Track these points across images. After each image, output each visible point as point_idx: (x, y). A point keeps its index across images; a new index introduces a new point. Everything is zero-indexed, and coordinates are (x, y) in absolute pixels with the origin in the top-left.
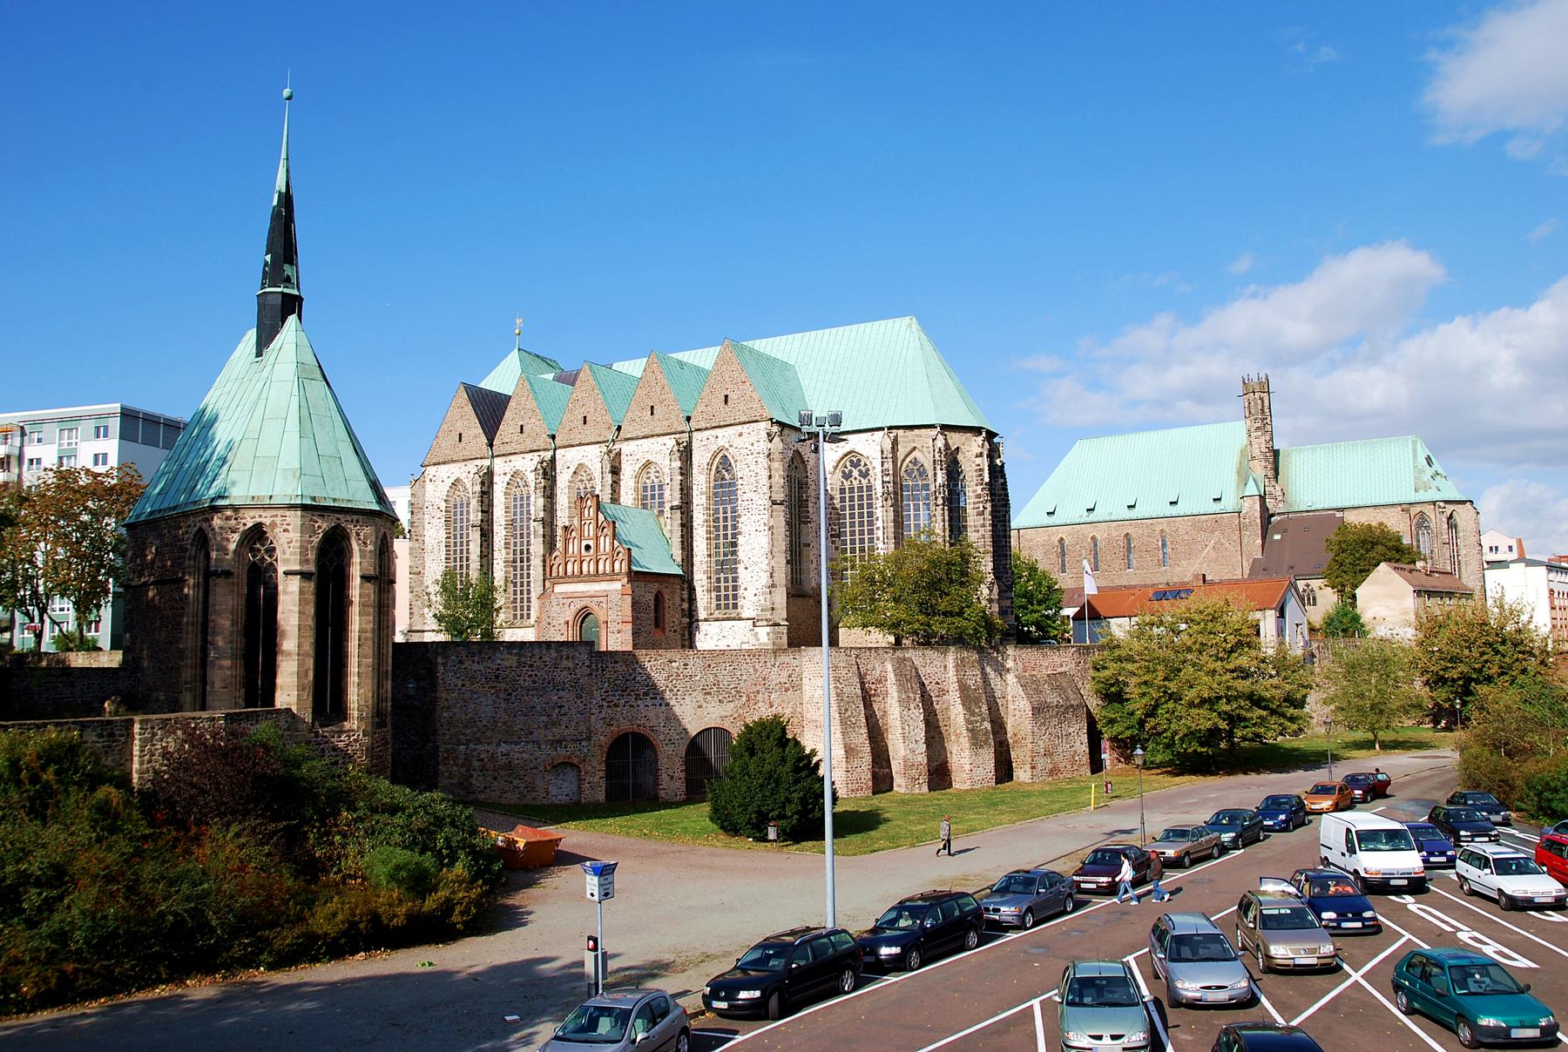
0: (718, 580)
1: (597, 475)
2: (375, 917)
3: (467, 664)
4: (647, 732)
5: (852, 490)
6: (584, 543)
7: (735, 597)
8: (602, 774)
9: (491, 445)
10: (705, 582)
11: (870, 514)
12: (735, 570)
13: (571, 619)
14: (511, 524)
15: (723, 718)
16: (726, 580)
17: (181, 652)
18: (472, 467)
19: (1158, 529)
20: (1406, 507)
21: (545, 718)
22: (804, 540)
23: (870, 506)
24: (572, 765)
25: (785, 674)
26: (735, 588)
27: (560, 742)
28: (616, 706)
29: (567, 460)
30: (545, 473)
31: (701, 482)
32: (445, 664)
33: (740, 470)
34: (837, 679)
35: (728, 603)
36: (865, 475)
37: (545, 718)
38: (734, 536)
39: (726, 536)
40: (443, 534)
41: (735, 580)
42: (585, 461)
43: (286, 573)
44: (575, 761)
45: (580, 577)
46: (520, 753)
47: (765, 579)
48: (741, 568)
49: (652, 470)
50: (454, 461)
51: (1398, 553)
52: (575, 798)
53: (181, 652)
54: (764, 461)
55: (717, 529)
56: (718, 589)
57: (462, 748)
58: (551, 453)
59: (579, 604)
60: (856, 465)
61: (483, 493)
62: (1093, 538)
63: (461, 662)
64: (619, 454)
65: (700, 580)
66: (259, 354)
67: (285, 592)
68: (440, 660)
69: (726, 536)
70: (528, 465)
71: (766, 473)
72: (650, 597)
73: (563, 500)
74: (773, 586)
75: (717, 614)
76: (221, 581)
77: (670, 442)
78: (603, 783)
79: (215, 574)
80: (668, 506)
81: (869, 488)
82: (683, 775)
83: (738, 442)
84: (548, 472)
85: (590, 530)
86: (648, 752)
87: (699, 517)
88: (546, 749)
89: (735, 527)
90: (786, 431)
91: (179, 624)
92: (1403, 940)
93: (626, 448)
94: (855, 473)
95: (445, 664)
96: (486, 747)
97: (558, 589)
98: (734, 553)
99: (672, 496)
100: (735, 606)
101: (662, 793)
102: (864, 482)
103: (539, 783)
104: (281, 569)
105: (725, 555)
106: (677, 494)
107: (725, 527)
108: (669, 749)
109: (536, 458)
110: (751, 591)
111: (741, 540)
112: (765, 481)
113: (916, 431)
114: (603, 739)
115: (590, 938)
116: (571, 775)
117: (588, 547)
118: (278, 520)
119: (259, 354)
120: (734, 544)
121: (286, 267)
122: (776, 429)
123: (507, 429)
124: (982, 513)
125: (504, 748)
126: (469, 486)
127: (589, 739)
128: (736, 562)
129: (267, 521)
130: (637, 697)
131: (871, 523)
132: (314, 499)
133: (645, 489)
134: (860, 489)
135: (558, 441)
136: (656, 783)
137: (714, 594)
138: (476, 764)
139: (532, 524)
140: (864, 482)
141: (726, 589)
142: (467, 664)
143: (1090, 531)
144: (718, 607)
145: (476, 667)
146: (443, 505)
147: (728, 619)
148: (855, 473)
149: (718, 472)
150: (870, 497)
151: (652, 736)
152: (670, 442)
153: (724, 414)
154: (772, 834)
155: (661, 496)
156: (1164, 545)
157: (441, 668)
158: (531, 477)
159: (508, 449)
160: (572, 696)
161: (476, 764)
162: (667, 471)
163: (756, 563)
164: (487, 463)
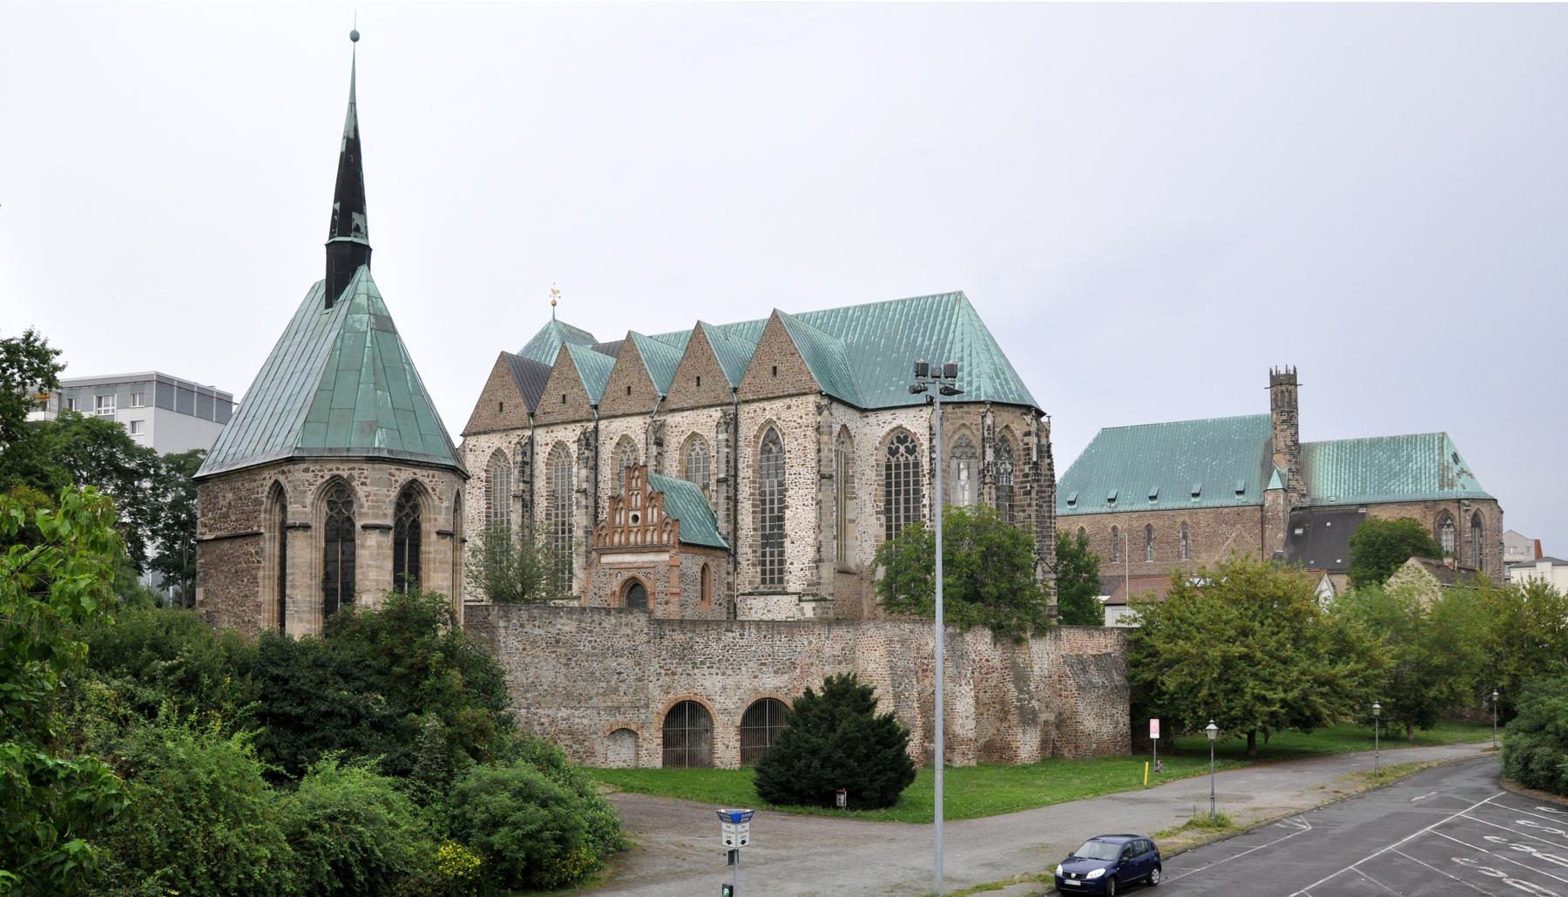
0: (764, 554)
1: (641, 446)
5: (898, 466)
7: (781, 571)
8: (660, 741)
10: (750, 556)
11: (917, 491)
12: (781, 545)
14: (552, 496)
15: (778, 689)
16: (772, 555)
17: (258, 606)
18: (514, 437)
19: (1179, 520)
20: (1429, 504)
22: (849, 516)
23: (916, 483)
24: (630, 732)
25: (838, 647)
26: (782, 562)
27: (618, 708)
28: (674, 674)
29: (611, 430)
30: (588, 444)
31: (748, 455)
33: (789, 443)
34: (891, 653)
35: (773, 578)
36: (911, 451)
38: (781, 510)
39: (772, 510)
40: (483, 504)
41: (781, 554)
43: (365, 527)
44: (633, 727)
46: (582, 719)
47: (811, 553)
48: (787, 543)
49: (697, 443)
50: (493, 431)
51: (1428, 551)
52: (632, 765)
53: (258, 606)
54: (811, 433)
55: (763, 502)
56: (763, 563)
57: (523, 711)
58: (592, 425)
59: (626, 575)
60: (902, 441)
61: (524, 463)
62: (1114, 528)
63: (522, 626)
64: (663, 425)
65: (746, 552)
66: (329, 305)
67: (363, 546)
68: (502, 624)
69: (772, 510)
70: (569, 435)
71: (812, 448)
72: (697, 569)
73: (606, 472)
74: (820, 560)
75: (762, 588)
76: (300, 533)
77: (716, 414)
78: (660, 750)
79: (294, 527)
80: (713, 481)
81: (916, 465)
82: (738, 744)
83: (785, 414)
84: (590, 442)
85: (637, 501)
86: (703, 720)
87: (745, 491)
88: (604, 715)
89: (781, 501)
90: (835, 405)
91: (255, 577)
93: (672, 419)
94: (902, 449)
95: (506, 628)
97: (605, 559)
98: (781, 527)
99: (718, 469)
100: (781, 581)
101: (717, 762)
102: (911, 459)
103: (599, 748)
104: (358, 525)
105: (772, 528)
106: (723, 467)
107: (772, 502)
111: (788, 514)
112: (812, 454)
113: (966, 409)
114: (661, 706)
115: (724, 886)
116: (628, 742)
117: (636, 518)
118: (356, 473)
119: (329, 305)
120: (781, 519)
121: (355, 215)
122: (825, 402)
123: (550, 400)
124: (1029, 493)
125: (564, 713)
126: (510, 456)
127: (647, 706)
128: (783, 536)
129: (345, 474)
130: (694, 666)
131: (917, 500)
132: (390, 452)
133: (689, 461)
134: (907, 466)
135: (602, 409)
136: (712, 752)
137: (759, 569)
138: (537, 728)
139: (575, 495)
140: (911, 459)
141: (772, 563)
142: (528, 628)
143: (1111, 522)
144: (763, 581)
145: (537, 631)
147: (774, 594)
148: (902, 449)
149: (764, 445)
150: (916, 474)
151: (708, 705)
152: (716, 414)
153: (771, 385)
154: (842, 799)
155: (706, 468)
156: (1185, 537)
157: (502, 631)
158: (573, 448)
159: (551, 419)
160: (630, 663)
161: (537, 728)
162: (712, 443)
163: (803, 538)
164: (529, 433)
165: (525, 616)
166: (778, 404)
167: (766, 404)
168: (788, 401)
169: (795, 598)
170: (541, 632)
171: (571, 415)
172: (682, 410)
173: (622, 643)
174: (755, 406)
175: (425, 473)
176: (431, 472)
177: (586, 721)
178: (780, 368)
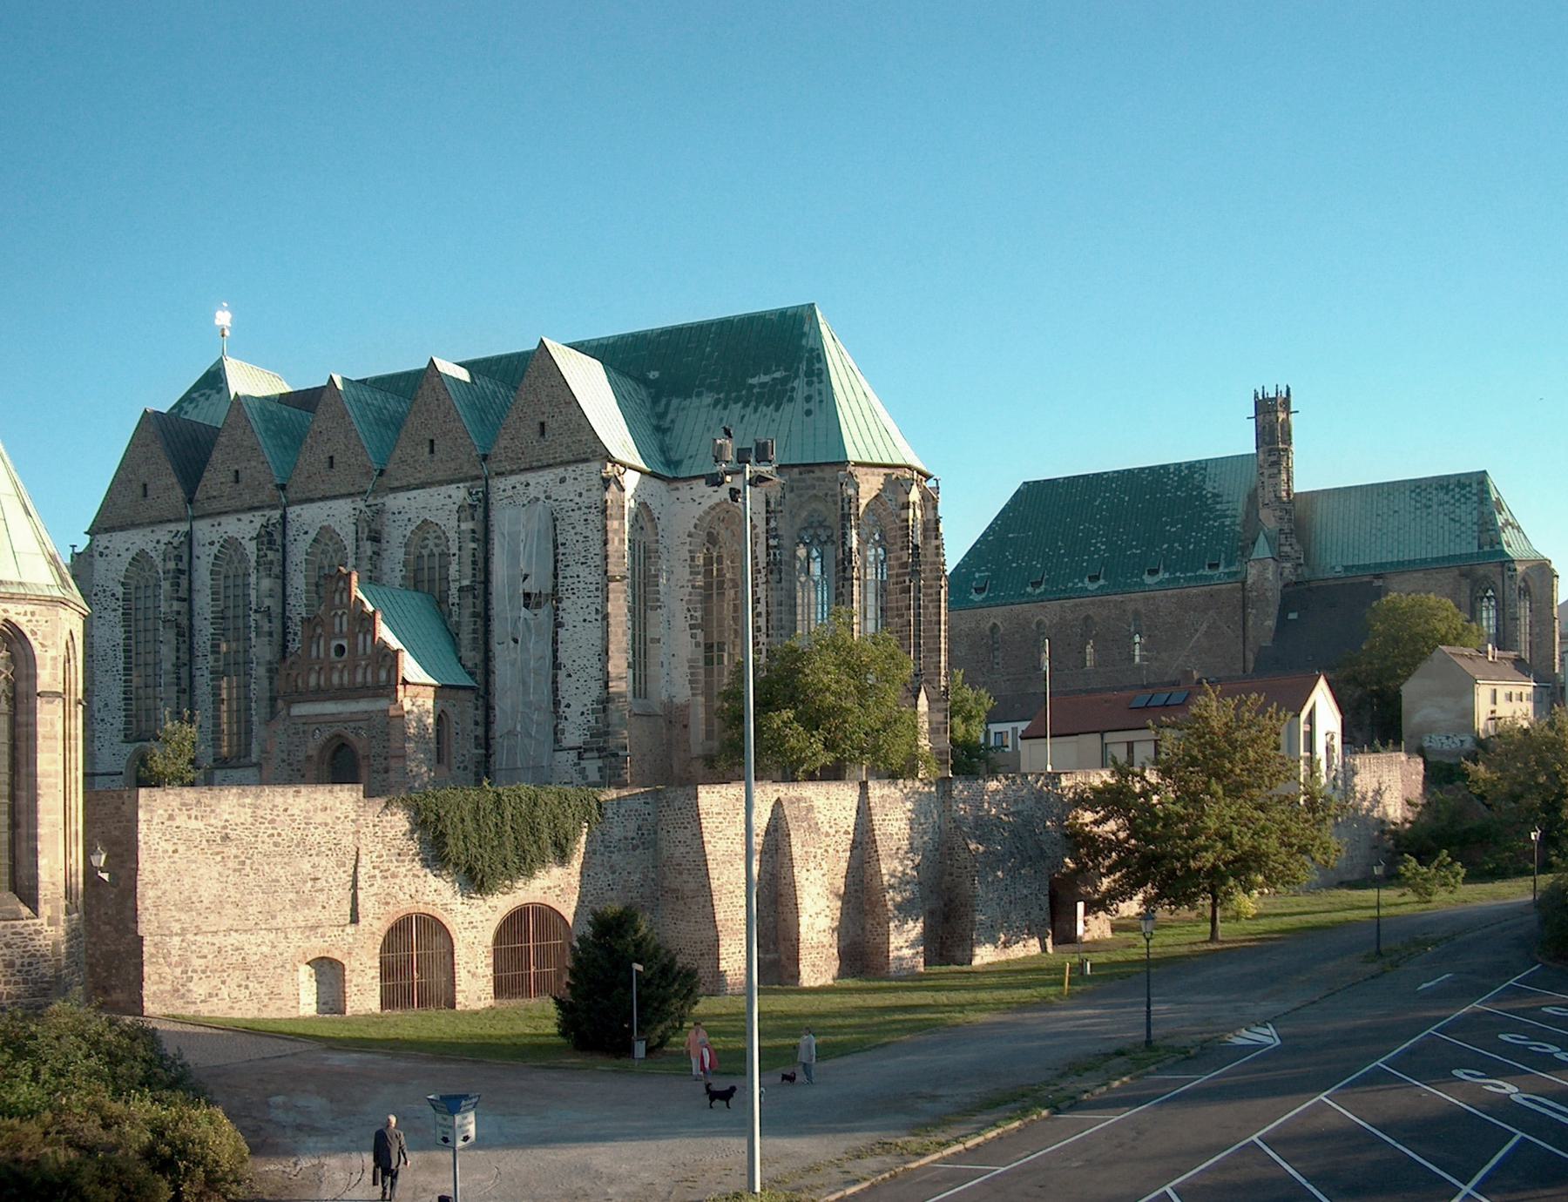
1: (349, 543)
2: (1355, 774)
3: (181, 820)
4: (439, 913)
6: (334, 643)
9: (190, 501)
13: (313, 753)
21: (292, 896)
22: (652, 633)
27: (314, 928)
28: (394, 876)
32: (149, 821)
37: (292, 896)
40: (119, 634)
42: (331, 522)
45: (321, 694)
57: (176, 940)
70: (243, 528)
77: (459, 493)
83: (559, 492)
88: (295, 937)
92: (1515, 1139)
93: (395, 502)
96: (210, 938)
108: (469, 935)
109: (258, 519)
110: (576, 707)
117: (340, 650)
123: (215, 479)
126: (158, 561)
142: (181, 820)
145: (193, 824)
146: (119, 591)
159: (216, 506)
162: (452, 535)
165: (176, 803)
166: (548, 476)
167: (531, 477)
168: (560, 471)
169: (573, 754)
170: (200, 825)
171: (248, 499)
172: (408, 488)
173: (317, 835)
174: (513, 479)
175: (21, 608)
176: (29, 608)
177: (265, 949)
178: (551, 424)
